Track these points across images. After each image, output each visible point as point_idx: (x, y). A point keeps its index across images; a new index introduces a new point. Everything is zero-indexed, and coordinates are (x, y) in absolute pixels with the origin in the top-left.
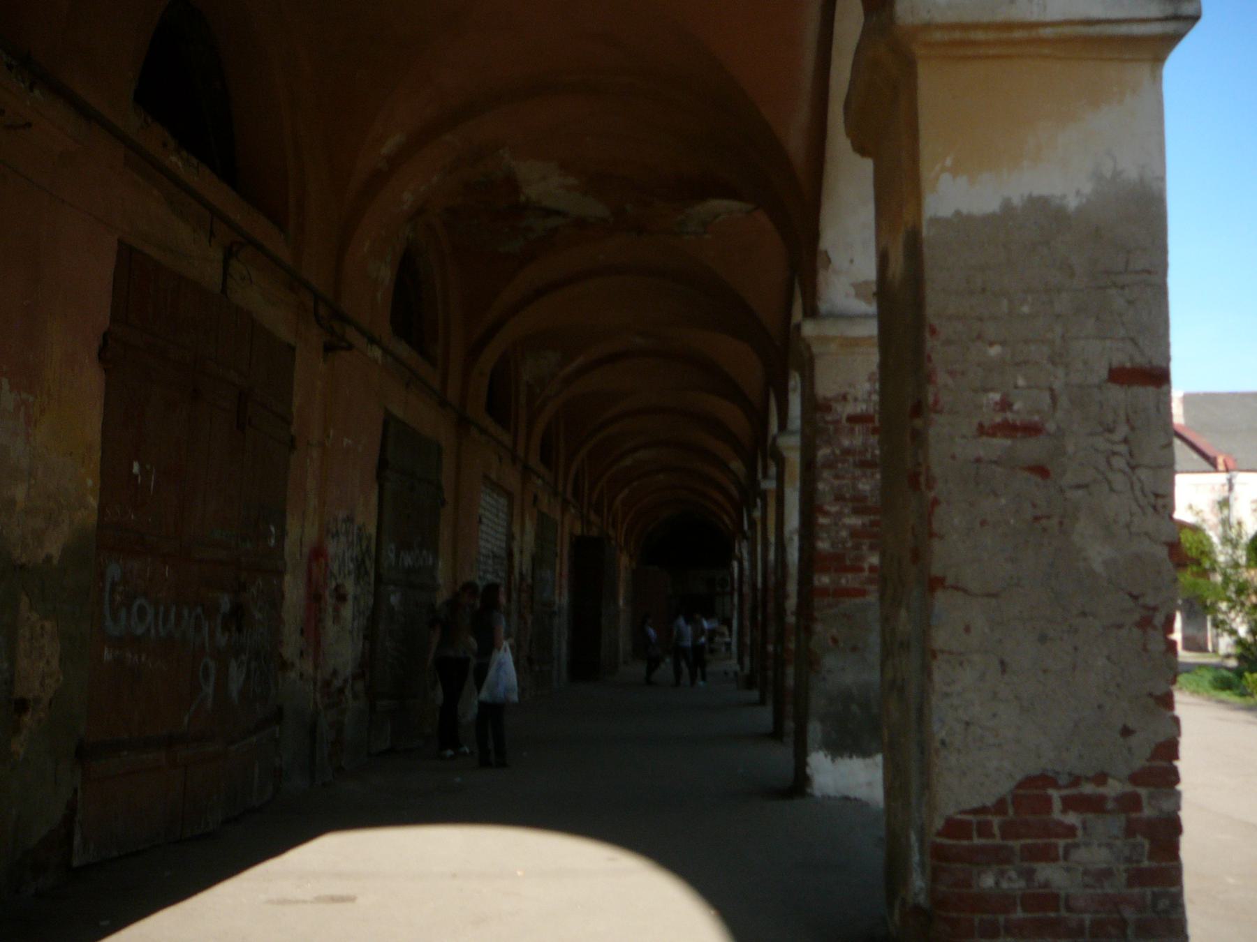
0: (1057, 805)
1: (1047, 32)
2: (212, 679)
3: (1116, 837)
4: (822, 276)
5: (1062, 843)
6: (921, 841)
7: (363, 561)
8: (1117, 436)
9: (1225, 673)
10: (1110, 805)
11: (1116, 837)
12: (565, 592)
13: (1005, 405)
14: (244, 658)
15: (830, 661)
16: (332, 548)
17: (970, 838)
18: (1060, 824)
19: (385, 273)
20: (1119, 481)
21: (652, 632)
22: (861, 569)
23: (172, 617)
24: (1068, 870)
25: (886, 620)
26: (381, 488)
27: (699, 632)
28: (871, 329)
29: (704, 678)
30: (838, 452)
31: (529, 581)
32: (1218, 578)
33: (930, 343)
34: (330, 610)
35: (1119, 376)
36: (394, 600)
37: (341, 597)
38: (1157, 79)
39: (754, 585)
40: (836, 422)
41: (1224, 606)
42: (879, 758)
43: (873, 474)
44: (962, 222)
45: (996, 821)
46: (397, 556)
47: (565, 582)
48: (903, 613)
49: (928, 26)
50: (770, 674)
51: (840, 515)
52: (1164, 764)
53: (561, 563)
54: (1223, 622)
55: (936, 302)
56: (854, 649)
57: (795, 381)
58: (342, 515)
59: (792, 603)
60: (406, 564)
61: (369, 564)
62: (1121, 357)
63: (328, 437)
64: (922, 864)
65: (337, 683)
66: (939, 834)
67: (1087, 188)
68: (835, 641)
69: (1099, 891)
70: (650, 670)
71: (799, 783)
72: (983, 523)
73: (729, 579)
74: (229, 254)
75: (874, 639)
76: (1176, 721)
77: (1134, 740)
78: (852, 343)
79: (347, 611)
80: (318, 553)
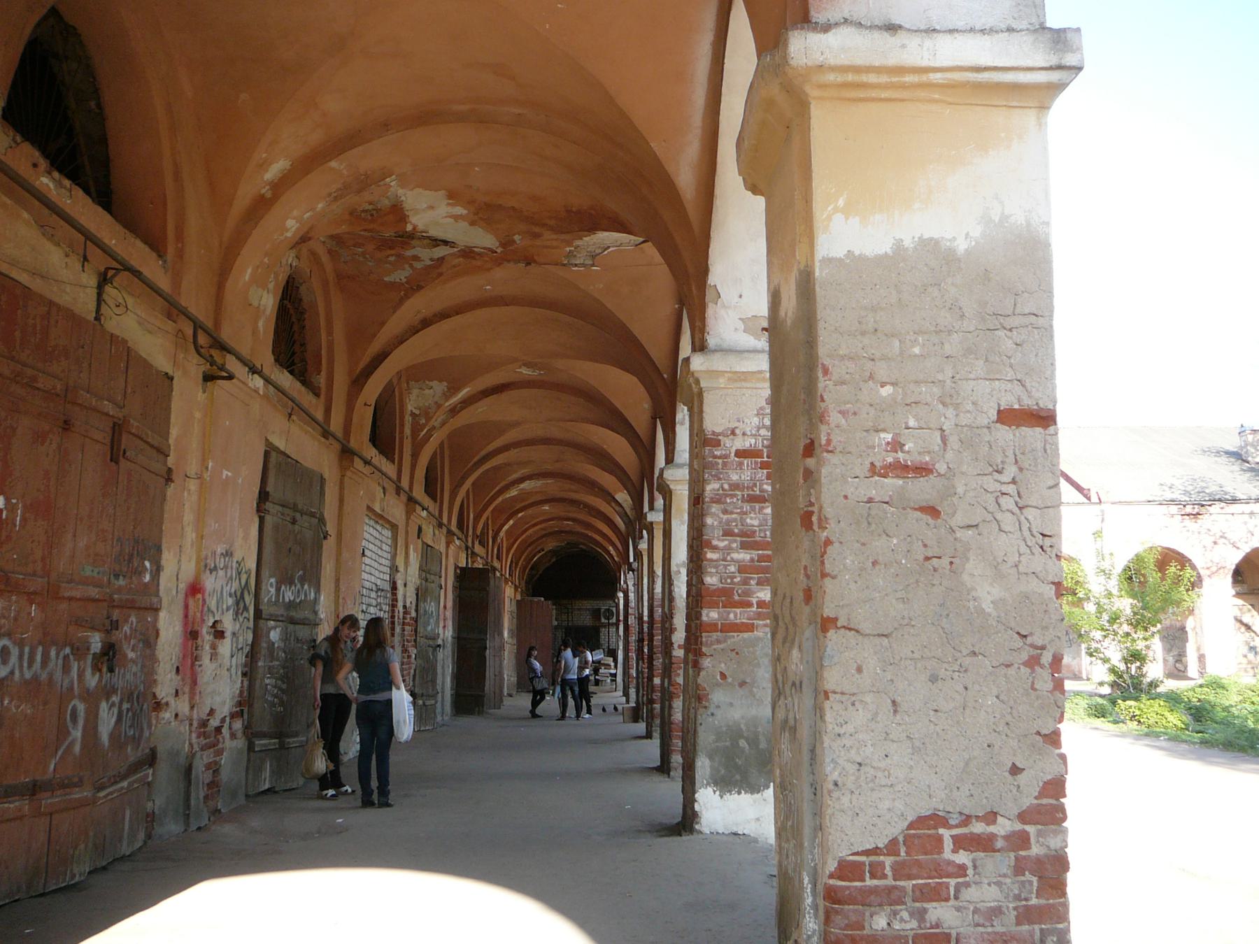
0: (948, 844)
1: (937, 77)
2: (81, 723)
3: (1005, 876)
4: (710, 311)
5: (952, 882)
7: (242, 594)
8: (1006, 477)
10: (1000, 844)
11: (1005, 876)
12: (450, 623)
14: (115, 699)
16: (209, 583)
17: (863, 880)
18: (950, 863)
19: (268, 302)
20: (1008, 521)
21: (537, 665)
22: (749, 605)
23: (39, 658)
24: (958, 909)
25: (777, 659)
26: (262, 521)
28: (762, 364)
29: (589, 712)
31: (413, 614)
32: (1090, 607)
33: (822, 383)
34: (207, 647)
35: (1008, 417)
36: (275, 635)
37: (220, 635)
38: (1041, 125)
41: (1098, 635)
43: (761, 509)
44: (854, 263)
45: (888, 861)
46: (278, 590)
47: (449, 614)
48: (795, 653)
50: (657, 706)
51: (728, 549)
52: (1052, 801)
54: (1096, 650)
57: (682, 414)
59: (679, 637)
61: (249, 600)
62: (1010, 400)
64: (815, 907)
65: (214, 723)
66: (831, 876)
67: (977, 232)
68: (723, 676)
69: (990, 929)
70: (535, 704)
71: (686, 822)
72: (875, 563)
73: (615, 611)
74: (104, 280)
75: (764, 675)
76: (1063, 758)
77: (1022, 778)
78: (742, 377)
79: (225, 647)
80: (195, 589)
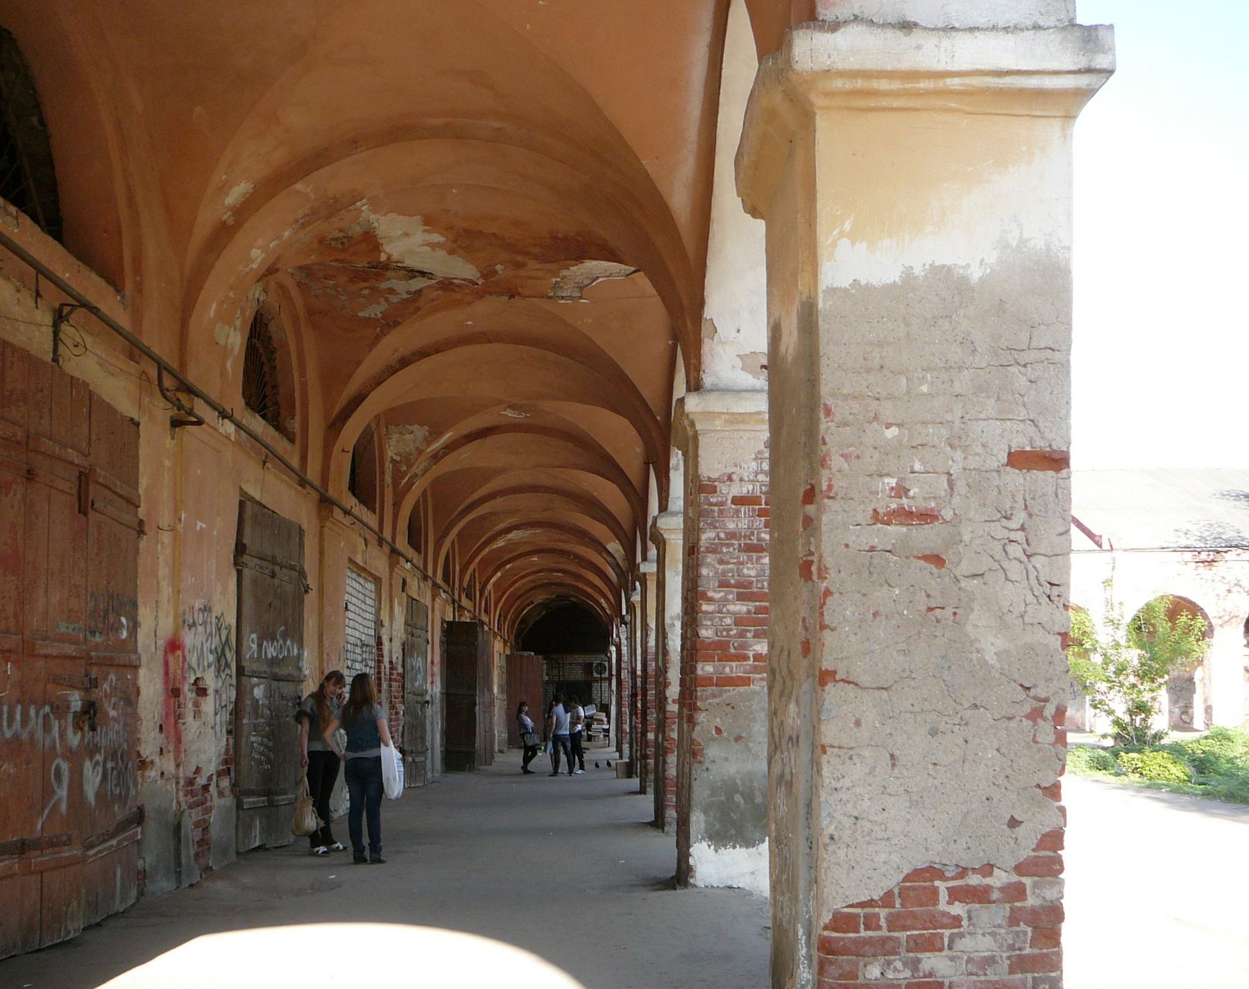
0: (943, 896)
2: (66, 781)
3: (999, 926)
6: (809, 936)
7: (223, 650)
8: (1014, 524)
9: (1103, 753)
10: (995, 895)
11: (999, 926)
12: (438, 679)
13: (901, 491)
14: (99, 757)
15: (712, 751)
16: (190, 639)
17: (858, 932)
18: (944, 914)
19: (236, 340)
20: (1015, 570)
21: (528, 721)
22: (746, 658)
23: (18, 717)
24: (952, 959)
27: (575, 720)
28: (761, 404)
29: (582, 767)
30: (722, 535)
31: (400, 670)
32: (1097, 658)
33: (824, 424)
34: (190, 705)
36: (258, 692)
37: (202, 692)
38: (1066, 137)
39: (633, 672)
40: (722, 504)
41: (1103, 686)
42: (765, 847)
43: (759, 558)
44: (860, 292)
45: (883, 913)
46: (260, 646)
48: (792, 707)
49: (828, 73)
50: (651, 762)
51: (725, 601)
52: (1050, 854)
53: (433, 652)
54: (1101, 702)
55: (831, 381)
56: (738, 739)
57: (676, 458)
58: (198, 604)
59: (673, 691)
60: (269, 656)
61: (230, 656)
62: (1021, 442)
63: (180, 520)
64: (809, 957)
65: (201, 781)
66: (826, 928)
67: (992, 258)
68: (718, 730)
70: (527, 760)
71: (681, 876)
72: (875, 614)
74: (59, 318)
75: (760, 729)
76: (1062, 810)
77: (1020, 831)
78: (738, 419)
79: (208, 705)
80: (174, 646)
